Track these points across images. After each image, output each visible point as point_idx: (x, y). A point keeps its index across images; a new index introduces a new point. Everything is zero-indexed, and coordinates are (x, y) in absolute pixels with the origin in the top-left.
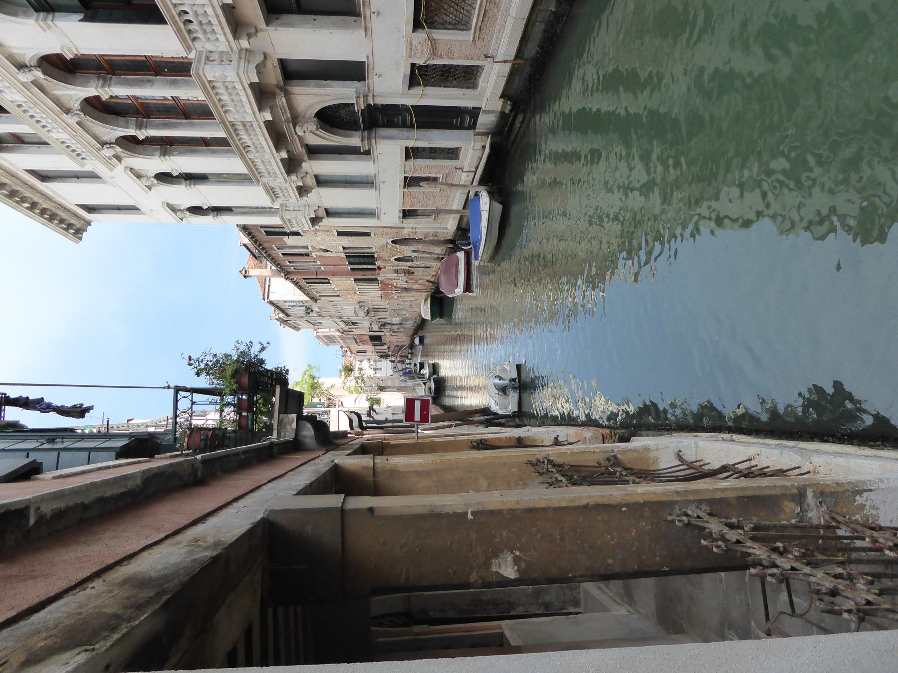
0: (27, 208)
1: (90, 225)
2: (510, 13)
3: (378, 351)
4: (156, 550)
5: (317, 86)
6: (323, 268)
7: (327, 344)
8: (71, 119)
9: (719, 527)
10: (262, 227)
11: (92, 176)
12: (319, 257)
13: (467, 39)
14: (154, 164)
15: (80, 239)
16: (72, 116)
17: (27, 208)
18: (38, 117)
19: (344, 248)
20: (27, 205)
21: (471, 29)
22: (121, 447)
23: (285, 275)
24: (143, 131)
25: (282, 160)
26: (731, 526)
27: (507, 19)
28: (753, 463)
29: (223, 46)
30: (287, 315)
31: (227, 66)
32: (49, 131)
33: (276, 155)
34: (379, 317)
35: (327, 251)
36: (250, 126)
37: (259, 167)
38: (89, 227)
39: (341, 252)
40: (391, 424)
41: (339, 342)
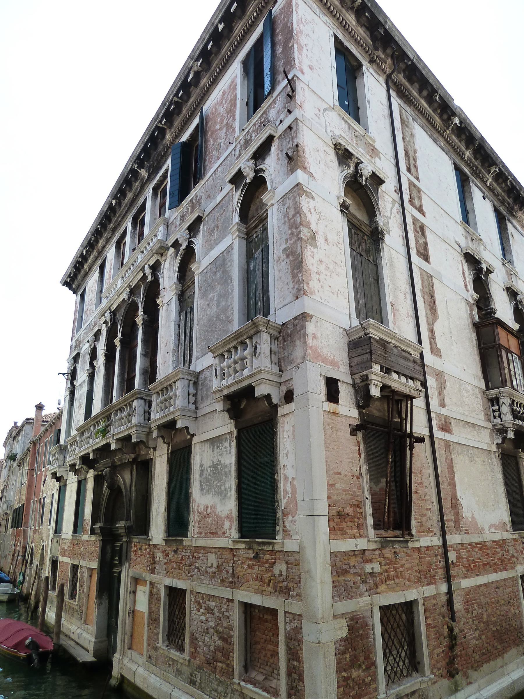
0: (82, 253)
4: (406, 272)
5: (235, 459)
6: (35, 476)
9: (196, 674)
11: (100, 300)
12: (42, 472)
14: (101, 346)
15: (64, 285)
17: (82, 253)
18: (129, 272)
20: (84, 253)
22: (468, 265)
28: (355, 614)
29: (154, 416)
31: (143, 417)
32: (123, 277)
33: (91, 450)
35: (44, 481)
39: (42, 495)
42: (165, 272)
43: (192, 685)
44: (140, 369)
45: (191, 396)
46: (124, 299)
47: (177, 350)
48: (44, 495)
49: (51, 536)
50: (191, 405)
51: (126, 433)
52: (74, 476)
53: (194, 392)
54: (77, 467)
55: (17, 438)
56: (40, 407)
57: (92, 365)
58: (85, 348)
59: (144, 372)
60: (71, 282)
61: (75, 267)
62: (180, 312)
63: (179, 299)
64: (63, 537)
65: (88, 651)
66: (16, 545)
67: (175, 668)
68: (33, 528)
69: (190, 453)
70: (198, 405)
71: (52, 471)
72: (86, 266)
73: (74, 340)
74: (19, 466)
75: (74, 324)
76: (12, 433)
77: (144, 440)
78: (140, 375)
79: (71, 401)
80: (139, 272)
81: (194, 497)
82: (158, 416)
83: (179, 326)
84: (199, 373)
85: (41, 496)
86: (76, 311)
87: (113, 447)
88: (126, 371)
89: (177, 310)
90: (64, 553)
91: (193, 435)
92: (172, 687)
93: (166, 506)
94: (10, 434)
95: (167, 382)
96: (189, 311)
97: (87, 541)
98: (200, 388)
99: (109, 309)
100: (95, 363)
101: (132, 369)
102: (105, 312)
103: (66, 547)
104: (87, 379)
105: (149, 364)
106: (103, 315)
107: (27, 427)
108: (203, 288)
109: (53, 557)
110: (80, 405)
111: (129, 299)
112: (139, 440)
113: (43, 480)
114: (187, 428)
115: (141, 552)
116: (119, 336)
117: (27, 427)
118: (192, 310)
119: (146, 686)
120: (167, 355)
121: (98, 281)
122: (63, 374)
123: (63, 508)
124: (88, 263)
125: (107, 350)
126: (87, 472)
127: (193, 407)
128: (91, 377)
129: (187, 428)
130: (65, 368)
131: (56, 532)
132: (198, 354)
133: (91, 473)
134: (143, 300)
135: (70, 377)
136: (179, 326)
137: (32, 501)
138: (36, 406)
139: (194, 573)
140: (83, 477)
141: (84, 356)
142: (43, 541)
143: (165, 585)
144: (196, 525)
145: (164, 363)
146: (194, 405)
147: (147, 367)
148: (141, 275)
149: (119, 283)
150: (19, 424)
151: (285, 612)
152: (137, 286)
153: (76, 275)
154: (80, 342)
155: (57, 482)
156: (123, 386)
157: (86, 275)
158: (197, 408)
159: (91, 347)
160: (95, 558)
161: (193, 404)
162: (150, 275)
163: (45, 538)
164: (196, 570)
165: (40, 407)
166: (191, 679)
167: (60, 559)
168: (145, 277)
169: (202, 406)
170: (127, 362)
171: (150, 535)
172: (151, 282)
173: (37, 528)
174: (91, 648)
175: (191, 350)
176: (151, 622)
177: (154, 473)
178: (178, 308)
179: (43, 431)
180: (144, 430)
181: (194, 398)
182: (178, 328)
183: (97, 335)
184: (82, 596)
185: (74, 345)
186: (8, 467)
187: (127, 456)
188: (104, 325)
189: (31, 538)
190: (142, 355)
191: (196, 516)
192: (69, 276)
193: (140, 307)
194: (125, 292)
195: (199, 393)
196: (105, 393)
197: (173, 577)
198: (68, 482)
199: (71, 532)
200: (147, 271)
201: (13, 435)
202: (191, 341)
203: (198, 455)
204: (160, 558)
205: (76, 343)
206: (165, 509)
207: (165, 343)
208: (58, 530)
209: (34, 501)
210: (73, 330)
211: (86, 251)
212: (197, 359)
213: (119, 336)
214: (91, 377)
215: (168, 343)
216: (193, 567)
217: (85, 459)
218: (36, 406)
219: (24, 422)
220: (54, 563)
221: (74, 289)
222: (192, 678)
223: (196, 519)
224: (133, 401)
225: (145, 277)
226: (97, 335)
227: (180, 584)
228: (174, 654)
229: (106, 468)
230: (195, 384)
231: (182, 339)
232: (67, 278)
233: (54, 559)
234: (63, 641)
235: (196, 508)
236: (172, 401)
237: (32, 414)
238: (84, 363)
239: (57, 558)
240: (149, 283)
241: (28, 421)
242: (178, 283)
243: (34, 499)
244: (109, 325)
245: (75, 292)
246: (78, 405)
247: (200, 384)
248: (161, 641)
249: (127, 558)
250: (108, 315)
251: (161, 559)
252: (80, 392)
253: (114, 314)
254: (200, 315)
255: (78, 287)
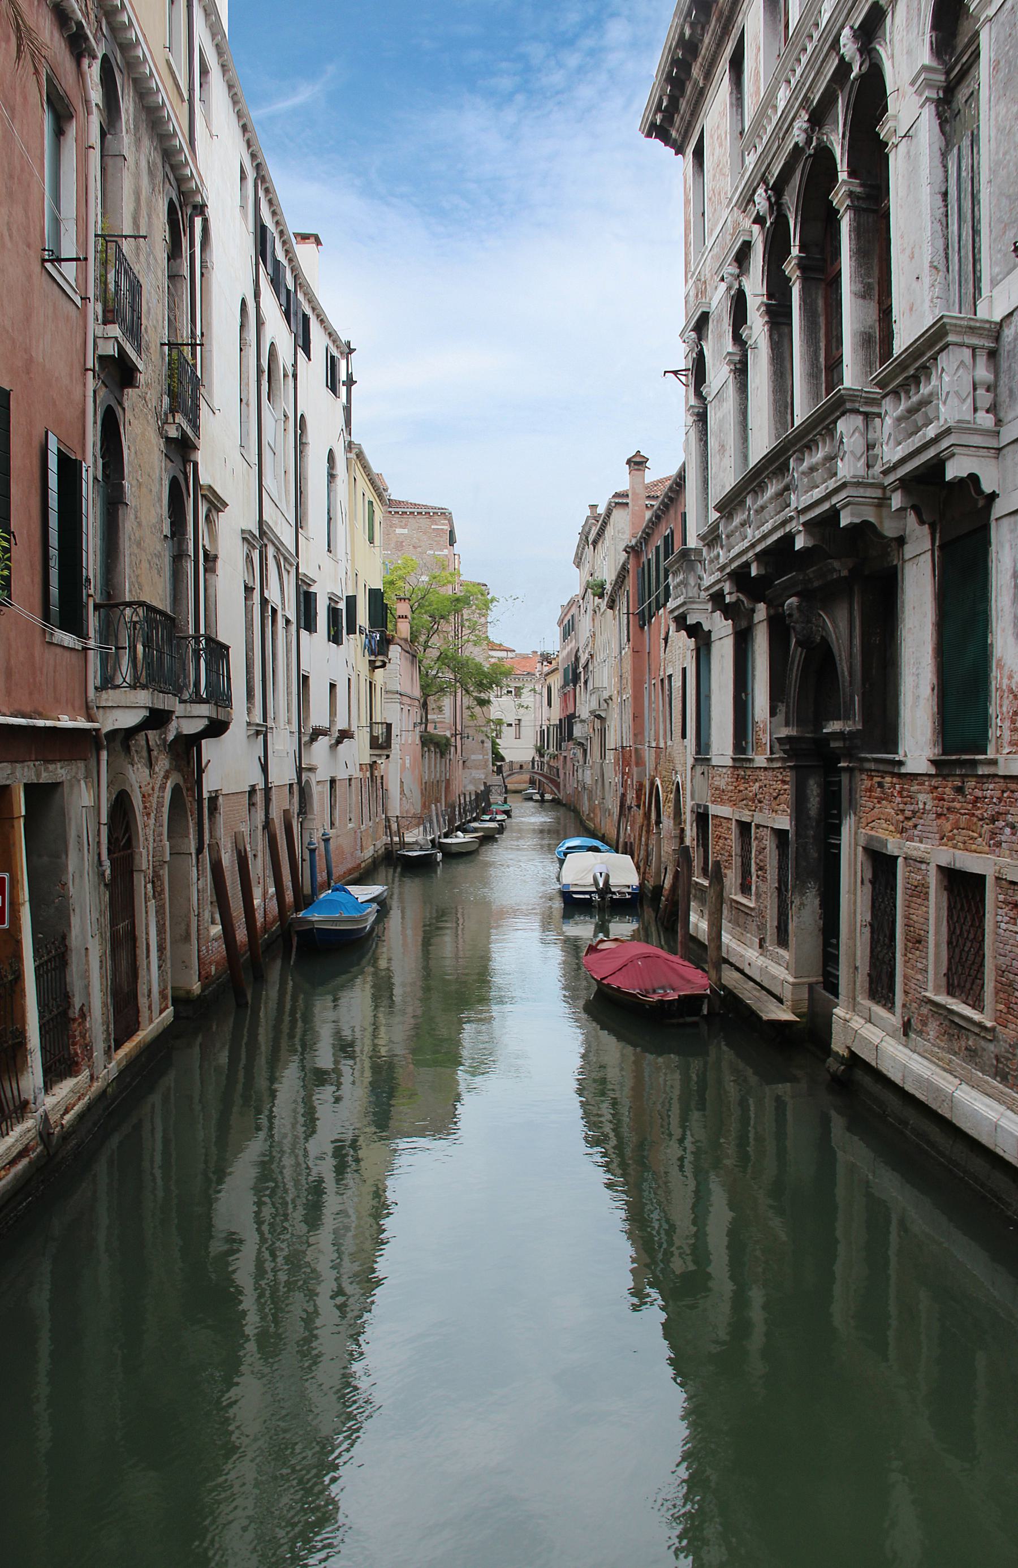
1: (676, 154)
2: (964, 1086)
3: (551, 730)
7: (560, 622)
8: (800, 128)
10: (978, 127)
13: (931, 985)
15: (649, 135)
16: (806, 131)
17: (682, 34)
19: (670, 676)
21: (950, 993)
23: (632, 547)
24: (798, 273)
25: (789, 539)
26: (660, 1247)
27: (956, 1077)
30: (595, 543)
34: (593, 739)
35: (666, 640)
36: (365, 1029)
37: (814, 453)
38: (673, 151)
40: (288, 1007)
41: (564, 648)
42: (897, 38)
43: (998, 1079)
44: (854, 335)
45: (981, 391)
46: (796, 144)
47: (942, 267)
48: (669, 672)
49: (690, 761)
50: (981, 414)
51: (826, 506)
52: (725, 623)
53: (989, 377)
54: (728, 600)
55: (600, 544)
56: (637, 463)
57: (738, 339)
58: (718, 299)
59: (866, 340)
60: (666, 125)
61: (669, 79)
62: (944, 155)
63: (939, 115)
64: (714, 763)
65: (780, 1001)
66: (624, 784)
67: (963, 1044)
68: (654, 745)
69: (986, 542)
70: (1002, 415)
71: (676, 613)
72: (696, 71)
73: (691, 282)
74: (611, 608)
75: (686, 236)
76: (589, 533)
77: (872, 520)
78: (854, 350)
79: (701, 440)
80: (827, 55)
81: (999, 655)
82: (900, 452)
83: (945, 195)
84: (1001, 324)
85: (662, 673)
86: (687, 202)
87: (800, 543)
88: (822, 345)
89: (936, 148)
90: (720, 796)
91: (993, 496)
92: (957, 1081)
93: (935, 682)
94: (584, 536)
95: (916, 360)
96: (966, 142)
97: (765, 769)
98: (1004, 365)
99: (764, 180)
100: (745, 333)
101: (835, 339)
102: (754, 191)
103: (723, 786)
104: (731, 380)
105: (876, 317)
106: (751, 200)
107: (618, 514)
108: (1002, 63)
109: (699, 806)
110: (722, 447)
111: (809, 141)
112: (857, 521)
113: (662, 636)
114: (974, 478)
115: (882, 792)
116: (795, 251)
117: (618, 514)
118: (975, 140)
119: (900, 1075)
120: (915, 284)
121: (731, 104)
122: (675, 373)
123: (708, 697)
124: (700, 60)
125: (770, 296)
126: (753, 611)
127: (986, 420)
128: (741, 370)
129: (974, 478)
130: (680, 357)
131: (698, 752)
132: (997, 270)
133: (761, 612)
134: (844, 137)
135: (692, 381)
136: (945, 195)
137: (646, 685)
138: (629, 462)
139: (1003, 838)
140: (744, 624)
141: (720, 320)
142: (676, 773)
143: (938, 866)
144: (1007, 724)
145: (911, 309)
146: (991, 416)
147: (870, 327)
148: (834, 63)
149: (783, 96)
150: (601, 510)
151: (997, 878)
152: (828, 99)
153: (674, 101)
154: (705, 282)
155: (690, 637)
156: (817, 386)
157: (701, 94)
158: (999, 422)
159: (732, 292)
160: (783, 806)
161: (987, 411)
162: (858, 57)
163: (679, 768)
164: (1008, 830)
165: (637, 463)
166: (997, 1067)
167: (714, 810)
168: (844, 67)
169: (1011, 415)
170: (822, 321)
171: (901, 752)
172: (861, 77)
173: (662, 745)
174: (787, 994)
175: (976, 261)
176: (910, 945)
177: (903, 602)
178: (939, 141)
179: (650, 520)
180: (869, 492)
181: (990, 396)
182: (941, 204)
183: (742, 256)
184: (763, 888)
185: (692, 293)
186: (590, 612)
187: (836, 564)
188: (756, 228)
189: (652, 767)
190: (856, 294)
191: (1006, 702)
192: (659, 109)
193: (838, 161)
194: (797, 124)
195: (1004, 379)
196: (775, 409)
197: (955, 847)
198: (714, 637)
199: (729, 751)
200: (848, 46)
201: (591, 538)
202: (976, 232)
203: (1007, 546)
204: (925, 804)
205: (697, 288)
206: (933, 689)
207: (908, 252)
208: (702, 745)
209: (650, 685)
210: (686, 254)
211: (693, 26)
212: (994, 283)
213: (795, 251)
214: (741, 370)
215: (917, 250)
216: (1001, 824)
217: (739, 577)
218: (629, 462)
219: (610, 504)
220: (702, 818)
221: (675, 140)
222: (1000, 1065)
223: (1004, 709)
224: (835, 422)
225: (844, 67)
226: (742, 256)
227: (971, 863)
228: (781, 952)
229: (791, 596)
230: (993, 354)
231: (953, 232)
232: (655, 114)
233: (701, 811)
234: (728, 977)
235: (1005, 681)
236: (930, 410)
237: (622, 480)
238: (720, 336)
239: (706, 807)
240: (857, 84)
241: (620, 501)
242: (934, 64)
243: (650, 682)
244: (768, 225)
245: (680, 150)
246: (717, 447)
247: (1003, 353)
248: (931, 985)
249: (853, 805)
250: (761, 197)
251: (927, 807)
252: (719, 415)
253: (778, 189)
254: (997, 153)
255: (686, 135)
